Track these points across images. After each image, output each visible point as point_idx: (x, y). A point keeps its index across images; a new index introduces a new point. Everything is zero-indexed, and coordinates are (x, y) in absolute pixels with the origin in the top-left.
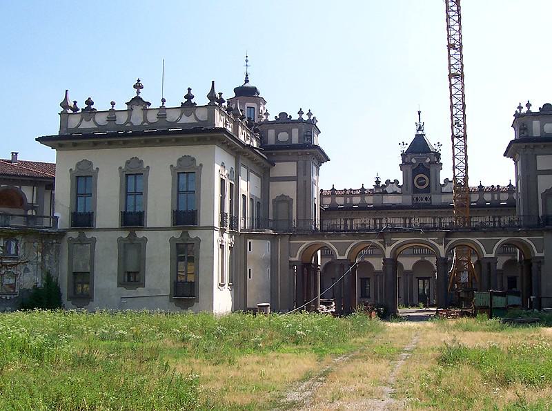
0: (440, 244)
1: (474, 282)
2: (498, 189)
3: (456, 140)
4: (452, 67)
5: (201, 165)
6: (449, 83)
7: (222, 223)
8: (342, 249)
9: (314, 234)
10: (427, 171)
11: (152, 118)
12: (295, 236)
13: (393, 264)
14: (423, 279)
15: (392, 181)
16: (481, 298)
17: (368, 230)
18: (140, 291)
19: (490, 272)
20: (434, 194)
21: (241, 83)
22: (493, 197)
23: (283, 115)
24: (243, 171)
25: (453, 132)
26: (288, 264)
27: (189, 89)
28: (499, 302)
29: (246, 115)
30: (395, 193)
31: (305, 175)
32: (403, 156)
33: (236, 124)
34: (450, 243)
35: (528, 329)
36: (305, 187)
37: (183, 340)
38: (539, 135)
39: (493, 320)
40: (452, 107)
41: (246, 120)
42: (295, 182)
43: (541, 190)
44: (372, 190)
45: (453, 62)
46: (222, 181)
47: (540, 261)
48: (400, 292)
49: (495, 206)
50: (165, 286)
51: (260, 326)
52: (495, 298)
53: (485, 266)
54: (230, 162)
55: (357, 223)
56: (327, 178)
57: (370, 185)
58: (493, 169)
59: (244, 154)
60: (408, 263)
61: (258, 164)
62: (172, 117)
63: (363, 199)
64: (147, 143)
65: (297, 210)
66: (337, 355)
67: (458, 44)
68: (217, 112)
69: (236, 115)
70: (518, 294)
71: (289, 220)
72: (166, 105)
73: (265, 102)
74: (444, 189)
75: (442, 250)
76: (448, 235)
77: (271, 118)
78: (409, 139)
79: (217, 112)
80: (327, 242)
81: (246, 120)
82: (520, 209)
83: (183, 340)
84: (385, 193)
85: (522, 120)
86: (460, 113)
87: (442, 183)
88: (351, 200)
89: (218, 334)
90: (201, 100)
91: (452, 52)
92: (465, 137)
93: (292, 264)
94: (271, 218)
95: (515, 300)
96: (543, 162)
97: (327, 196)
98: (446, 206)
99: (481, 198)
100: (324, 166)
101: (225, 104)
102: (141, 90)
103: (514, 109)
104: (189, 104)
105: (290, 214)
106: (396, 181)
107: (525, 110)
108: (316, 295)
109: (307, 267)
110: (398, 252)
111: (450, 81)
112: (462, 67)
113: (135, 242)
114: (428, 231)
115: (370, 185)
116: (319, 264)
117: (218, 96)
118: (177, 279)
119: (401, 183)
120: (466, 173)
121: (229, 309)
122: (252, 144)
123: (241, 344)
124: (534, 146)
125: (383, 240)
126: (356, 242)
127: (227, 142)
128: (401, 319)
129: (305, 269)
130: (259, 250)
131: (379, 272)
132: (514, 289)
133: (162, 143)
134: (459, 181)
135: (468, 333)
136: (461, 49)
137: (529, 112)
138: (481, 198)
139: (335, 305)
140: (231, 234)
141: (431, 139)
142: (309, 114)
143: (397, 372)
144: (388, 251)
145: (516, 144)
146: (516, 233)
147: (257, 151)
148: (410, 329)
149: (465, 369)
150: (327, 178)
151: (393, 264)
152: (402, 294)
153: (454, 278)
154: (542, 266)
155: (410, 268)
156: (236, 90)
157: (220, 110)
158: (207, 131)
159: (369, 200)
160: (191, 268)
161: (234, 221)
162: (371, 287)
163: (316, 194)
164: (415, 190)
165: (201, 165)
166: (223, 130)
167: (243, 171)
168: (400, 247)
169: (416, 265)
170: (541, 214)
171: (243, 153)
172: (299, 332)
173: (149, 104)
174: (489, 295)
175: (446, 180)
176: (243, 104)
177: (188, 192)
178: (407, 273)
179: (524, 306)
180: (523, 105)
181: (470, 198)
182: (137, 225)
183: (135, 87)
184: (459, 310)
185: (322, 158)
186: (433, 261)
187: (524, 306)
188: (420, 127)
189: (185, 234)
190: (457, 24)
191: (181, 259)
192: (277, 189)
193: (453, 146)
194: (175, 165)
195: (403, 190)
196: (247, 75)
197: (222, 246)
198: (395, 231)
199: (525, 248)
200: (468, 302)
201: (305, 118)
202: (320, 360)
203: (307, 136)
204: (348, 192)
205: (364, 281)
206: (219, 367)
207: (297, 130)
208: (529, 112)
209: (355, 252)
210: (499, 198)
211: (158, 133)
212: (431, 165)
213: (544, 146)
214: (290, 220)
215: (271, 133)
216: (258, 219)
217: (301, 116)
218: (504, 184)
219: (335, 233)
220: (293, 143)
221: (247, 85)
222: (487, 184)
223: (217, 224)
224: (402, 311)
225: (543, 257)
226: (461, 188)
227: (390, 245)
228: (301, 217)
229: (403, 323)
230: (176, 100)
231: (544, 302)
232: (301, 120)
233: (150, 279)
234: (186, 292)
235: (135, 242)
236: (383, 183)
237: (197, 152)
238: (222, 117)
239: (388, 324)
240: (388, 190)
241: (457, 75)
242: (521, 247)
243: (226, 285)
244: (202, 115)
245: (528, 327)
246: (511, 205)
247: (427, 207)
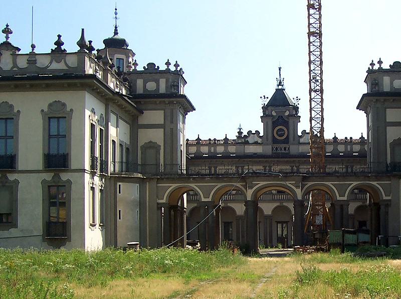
0: (297, 187)
1: (328, 224)
2: (351, 141)
3: (313, 94)
4: (311, 26)
5: (72, 110)
6: (308, 68)
7: (93, 166)
8: (206, 191)
9: (180, 178)
10: (286, 124)
11: (22, 63)
12: (163, 179)
13: (253, 206)
14: (282, 223)
15: (254, 132)
16: (334, 235)
17: (231, 174)
18: (13, 232)
19: (342, 214)
20: (293, 144)
21: (110, 35)
22: (346, 148)
23: (151, 65)
24: (113, 117)
25: (310, 86)
26: (156, 205)
27: (59, 36)
28: (351, 239)
29: (115, 64)
30: (256, 143)
31: (172, 122)
32: (265, 108)
33: (105, 72)
34: (306, 187)
35: (375, 261)
36: (172, 135)
37: (57, 271)
38: (389, 90)
39: (344, 255)
40: (310, 62)
41: (115, 68)
42: (163, 130)
43: (390, 140)
44: (235, 140)
45: (312, 21)
46: (92, 126)
47: (388, 204)
48: (260, 234)
49: (348, 156)
50: (38, 226)
51: (130, 260)
52: (347, 236)
53: (339, 208)
54: (100, 109)
55: (221, 169)
56: (196, 128)
57: (233, 136)
58: (346, 123)
59: (112, 100)
60: (267, 208)
61: (126, 111)
62: (42, 63)
63: (226, 149)
64: (17, 88)
65: (164, 157)
66: (201, 280)
67: (318, 4)
68: (87, 59)
69: (106, 63)
70: (369, 232)
71: (156, 165)
72: (36, 51)
73: (134, 54)
74: (302, 140)
75: (299, 193)
76: (305, 179)
77: (140, 68)
78: (270, 93)
79: (87, 59)
80: (193, 185)
81: (115, 68)
82: (371, 158)
83: (57, 271)
84: (247, 143)
85: (374, 76)
86: (317, 68)
87: (300, 134)
88: (215, 150)
89: (91, 266)
90: (71, 46)
91: (312, 11)
92: (322, 91)
93: (159, 206)
94: (139, 163)
95: (364, 237)
96: (392, 115)
97: (192, 145)
98: (304, 156)
99: (335, 149)
100: (190, 115)
101: (95, 52)
102: (10, 35)
103: (367, 66)
104: (59, 51)
105: (158, 159)
106: (257, 132)
107: (376, 67)
108: (182, 234)
109: (174, 209)
110: (259, 195)
111: (309, 39)
112: (320, 26)
113: (7, 184)
114: (287, 176)
115: (233, 136)
116: (185, 206)
117: (88, 43)
118: (49, 218)
119: (262, 134)
120: (322, 125)
121: (101, 248)
122: (121, 92)
123: (112, 274)
124: (385, 100)
125: (244, 184)
126: (219, 185)
127: (97, 89)
128: (261, 256)
129: (172, 211)
130: (128, 192)
131: (240, 217)
132: (364, 228)
133: (33, 88)
134: (316, 133)
135: (322, 264)
136: (320, 9)
137: (380, 69)
138: (335, 149)
139: (201, 246)
140: (101, 177)
141: (291, 94)
142: (177, 65)
143: (258, 290)
144: (249, 194)
145: (368, 98)
146: (369, 178)
147: (126, 98)
148: (269, 262)
149: (320, 286)
150: (196, 128)
151: (253, 206)
152: (262, 239)
153: (309, 222)
154: (389, 208)
155: (270, 213)
156: (105, 42)
157: (90, 58)
158: (77, 77)
159: (232, 149)
160: (62, 213)
161: (104, 165)
162: (233, 230)
163: (182, 142)
164: (275, 141)
165: (72, 110)
166: (93, 77)
167: (113, 117)
168: (259, 191)
169: (275, 210)
170: (389, 161)
171: (113, 100)
172: (167, 262)
173: (19, 50)
174: (341, 233)
175: (304, 132)
176: (112, 55)
177: (58, 136)
178: (267, 217)
179: (372, 242)
180: (376, 62)
181: (325, 149)
182: (9, 168)
183: (4, 31)
184: (314, 247)
185: (188, 107)
186: (291, 206)
187: (372, 242)
188: (280, 82)
189: (57, 176)
190: (318, 13)
191: (53, 204)
192: (146, 136)
193: (311, 100)
194: (46, 110)
195: (263, 141)
196: (116, 27)
197: (93, 189)
198: (256, 175)
199: (375, 192)
200: (322, 242)
201: (172, 68)
202: (187, 283)
203: (174, 86)
204: (212, 142)
205: (227, 225)
206: (93, 289)
207: (164, 80)
208: (380, 69)
209: (219, 195)
210: (352, 149)
211: (28, 78)
212: (290, 118)
213: (394, 100)
214: (158, 165)
215: (140, 83)
216: (127, 163)
217: (168, 67)
218: (357, 137)
219: (201, 177)
220: (160, 92)
221: (116, 37)
222: (341, 137)
223: (87, 166)
224: (261, 251)
225: (390, 200)
226: (317, 139)
227: (251, 188)
228: (168, 162)
229: (263, 258)
230: (46, 46)
231: (391, 240)
232: (168, 71)
233: (23, 220)
234: (59, 232)
235: (7, 184)
236: (245, 133)
237: (66, 97)
238: (92, 65)
239: (249, 259)
240: (250, 140)
241: (315, 34)
242: (371, 192)
243: (97, 226)
244: (72, 62)
245: (376, 259)
246: (363, 155)
247: (286, 157)
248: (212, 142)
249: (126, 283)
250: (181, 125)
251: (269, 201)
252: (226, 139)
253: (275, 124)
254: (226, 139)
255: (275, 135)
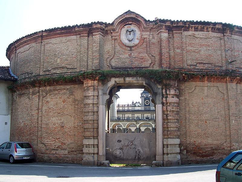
0: (153, 124)
57: (130, 103)
80: (120, 123)
84: (136, 106)
106: (139, 102)
126: (128, 123)
144: (138, 126)
159: (130, 108)
164: (145, 105)
227: (138, 124)
240: (137, 105)
251: (143, 126)
252: (128, 105)
253: (145, 99)
254: (128, 105)
255: (145, 103)
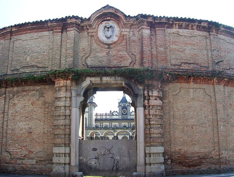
0: (130, 132)
9: (93, 129)
15: (115, 111)
31: (91, 111)
32: (119, 103)
57: (108, 112)
63: (106, 117)
74: (132, 114)
84: (113, 115)
88: (102, 117)
100: (96, 108)
126: (106, 131)
159: (108, 117)
164: (123, 114)
204: (101, 115)
240: (114, 114)
248: (101, 115)
249: (124, 147)
250: (93, 111)
252: (106, 114)
253: (123, 109)
